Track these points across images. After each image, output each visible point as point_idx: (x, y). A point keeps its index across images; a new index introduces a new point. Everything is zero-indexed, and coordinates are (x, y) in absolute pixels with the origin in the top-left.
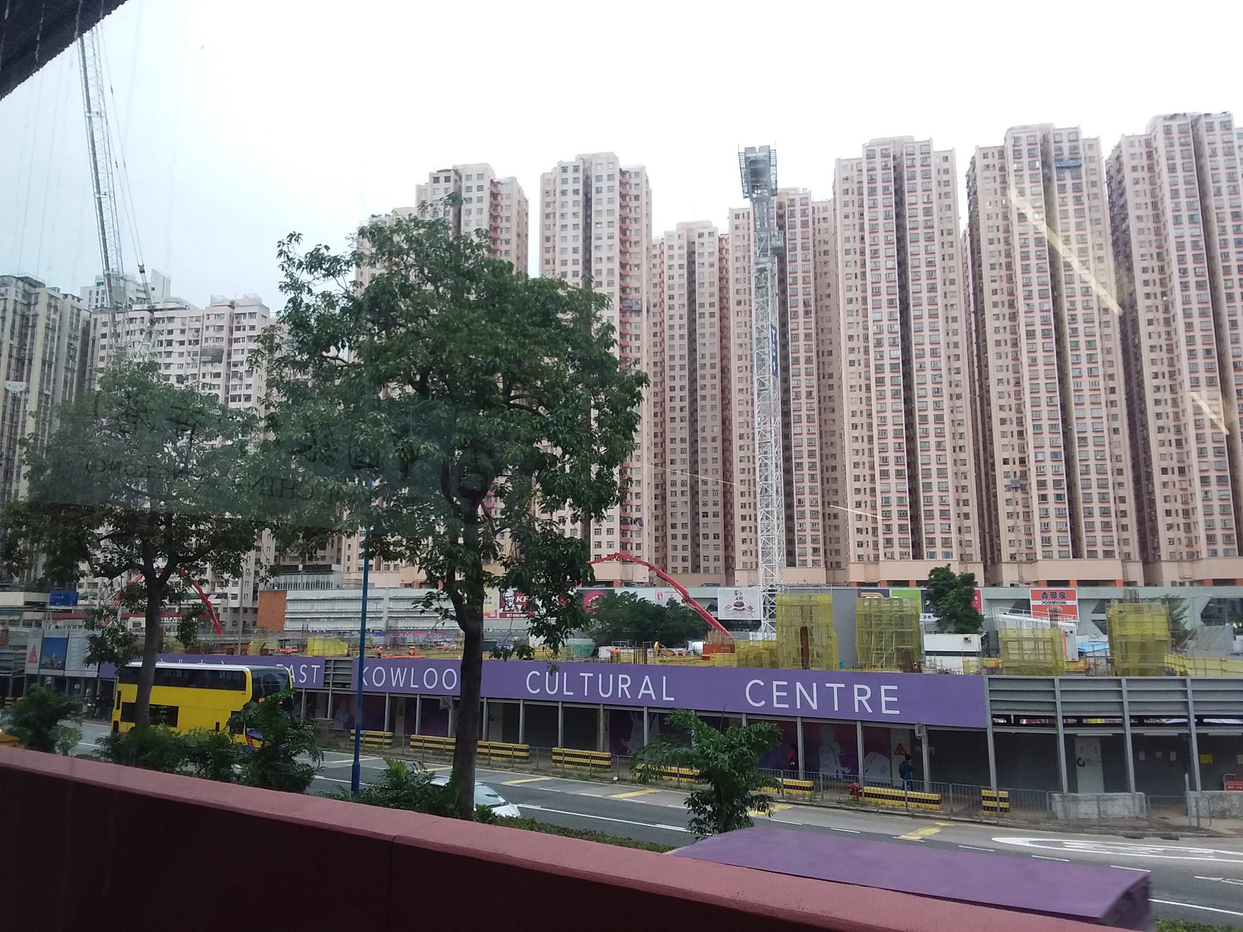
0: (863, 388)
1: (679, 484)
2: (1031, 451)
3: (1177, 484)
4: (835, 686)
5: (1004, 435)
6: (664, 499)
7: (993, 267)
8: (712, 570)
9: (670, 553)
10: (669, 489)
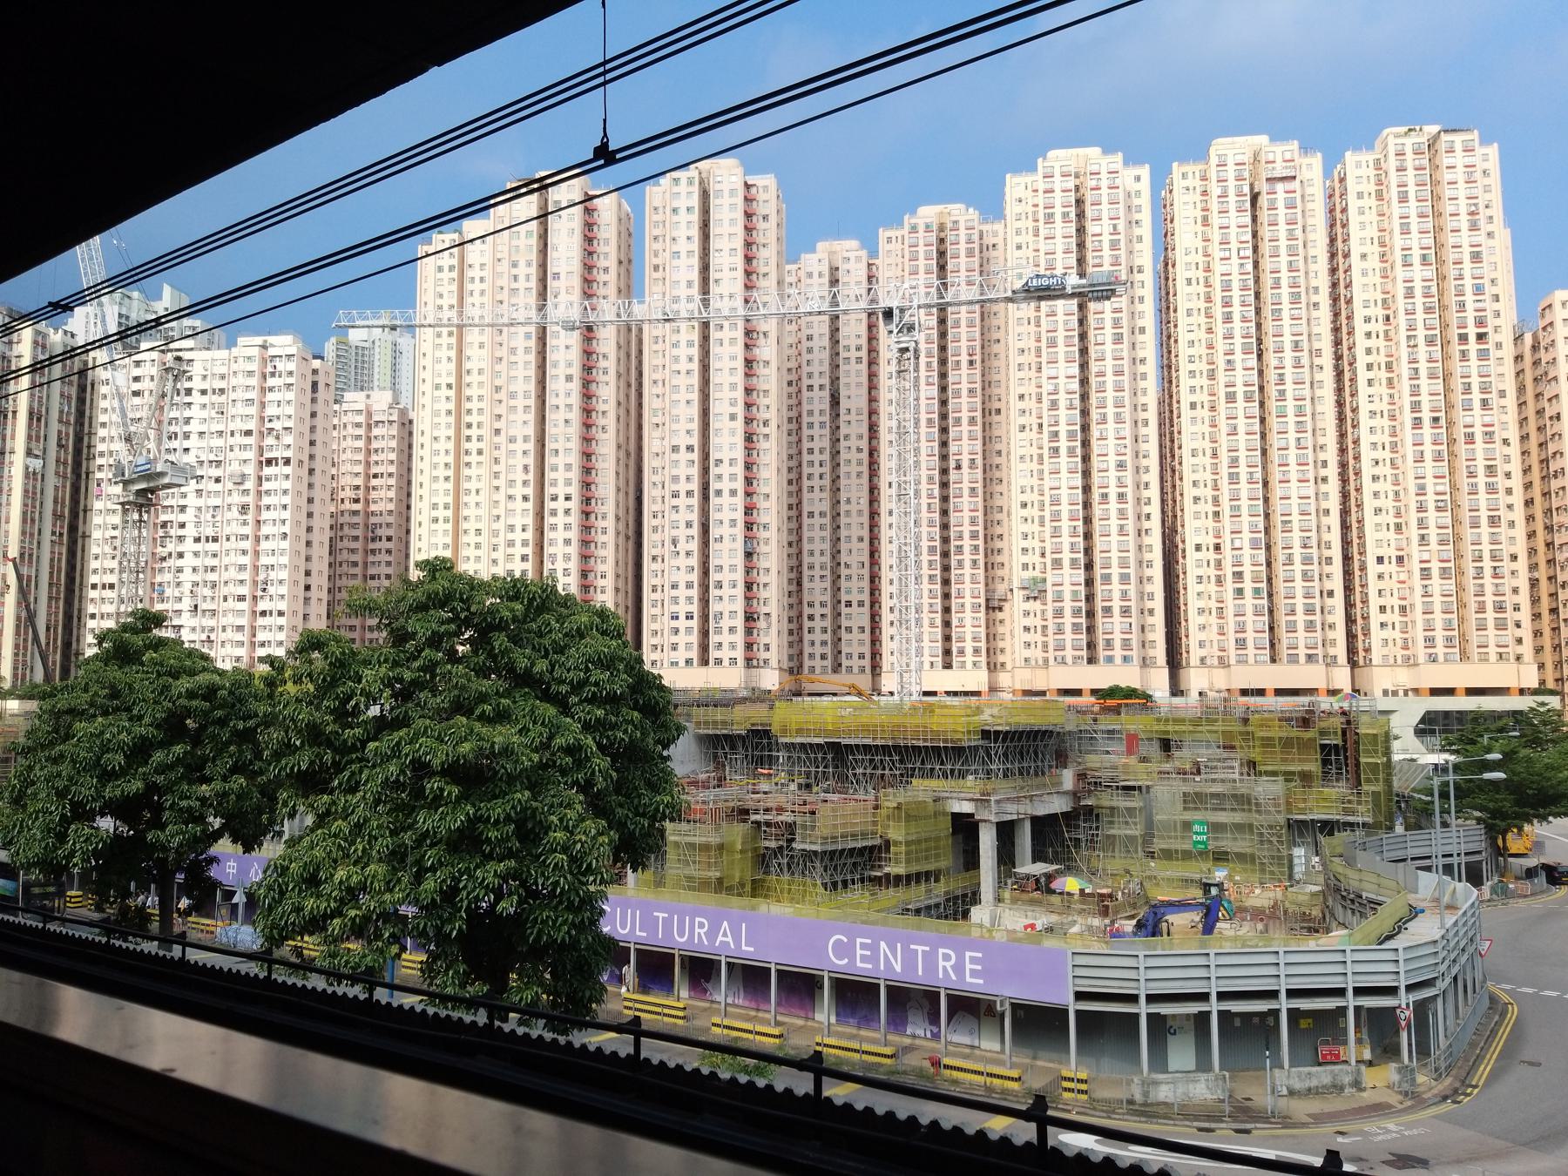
0: (1035, 458)
1: (817, 567)
2: (1227, 537)
4: (920, 948)
5: (1197, 515)
6: (799, 584)
7: (1189, 313)
8: (855, 670)
9: (807, 650)
10: (806, 573)
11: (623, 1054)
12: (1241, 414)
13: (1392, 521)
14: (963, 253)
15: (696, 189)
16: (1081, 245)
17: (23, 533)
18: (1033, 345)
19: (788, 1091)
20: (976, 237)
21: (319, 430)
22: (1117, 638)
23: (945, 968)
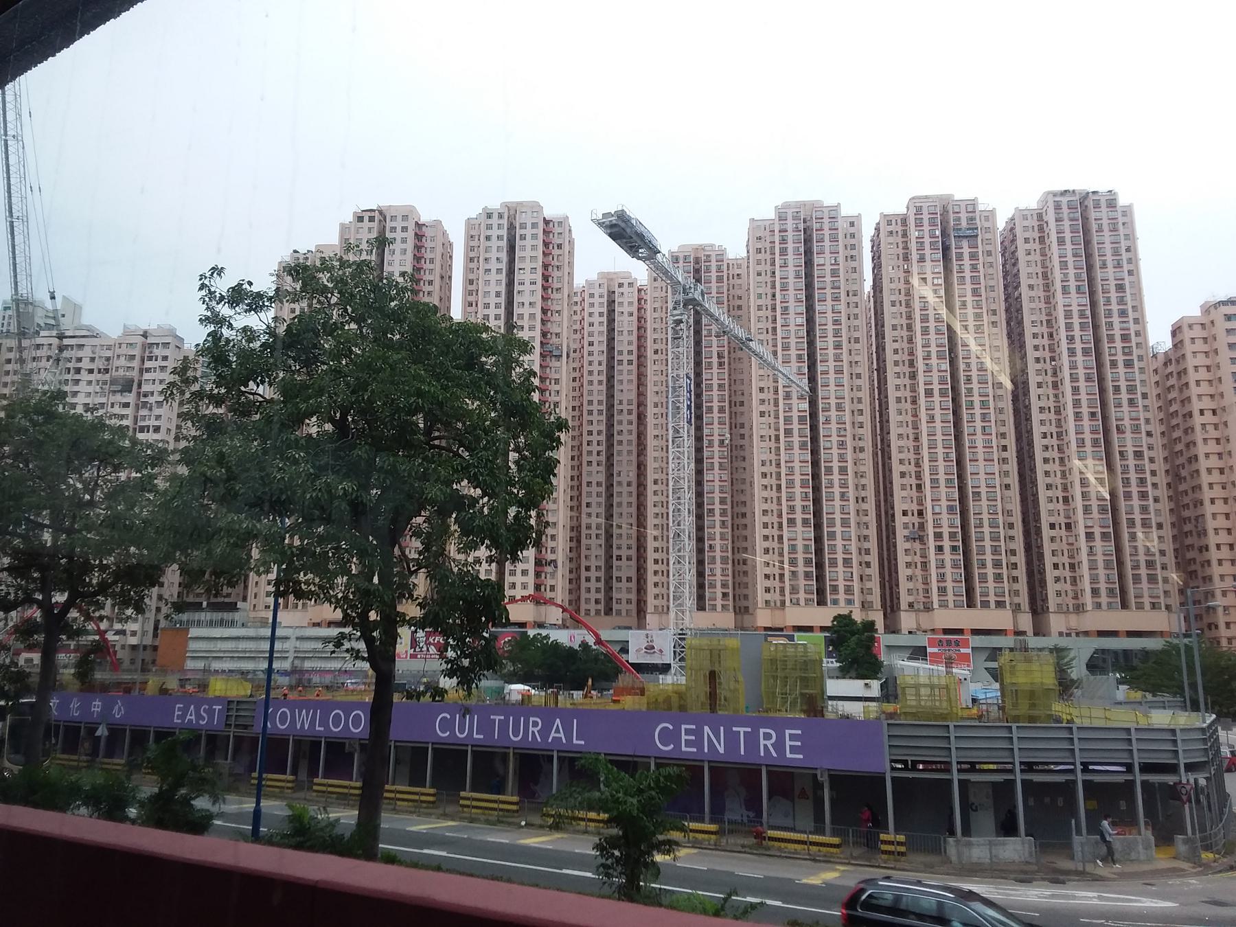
3: (1064, 539)
4: (742, 730)
8: (624, 613)
9: (584, 595)
10: (584, 531)
23: (765, 746)
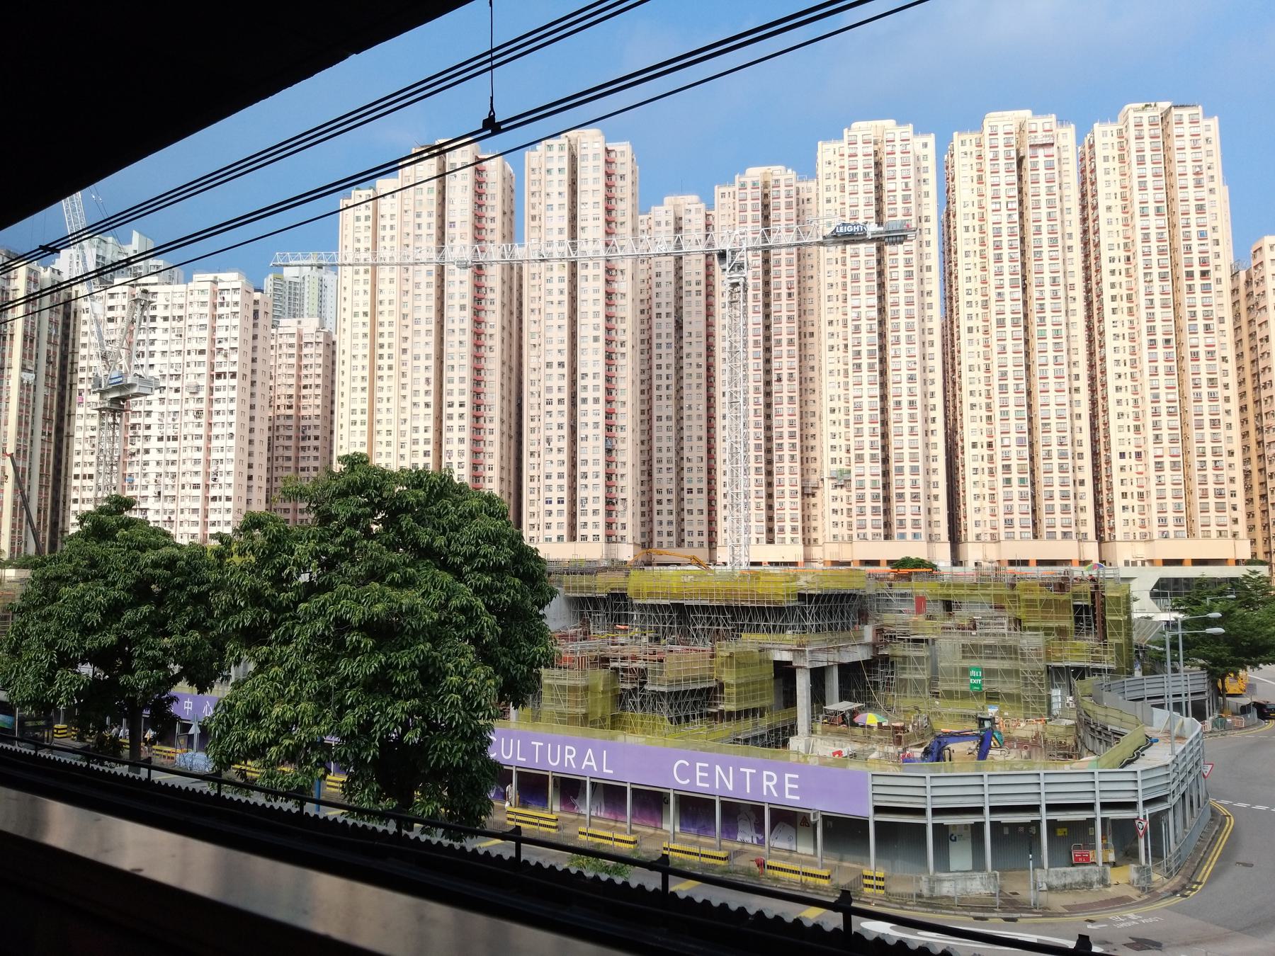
0: (842, 372)
1: (665, 461)
2: (998, 436)
4: (748, 771)
5: (973, 419)
6: (650, 475)
7: (967, 254)
8: (696, 545)
9: (656, 528)
10: (655, 465)
11: (506, 857)
12: (1009, 336)
13: (1132, 423)
14: (783, 206)
15: (566, 153)
16: (879, 200)
17: (19, 433)
18: (840, 280)
19: (641, 887)
20: (793, 193)
21: (259, 349)
22: (909, 519)
23: (768, 787)
